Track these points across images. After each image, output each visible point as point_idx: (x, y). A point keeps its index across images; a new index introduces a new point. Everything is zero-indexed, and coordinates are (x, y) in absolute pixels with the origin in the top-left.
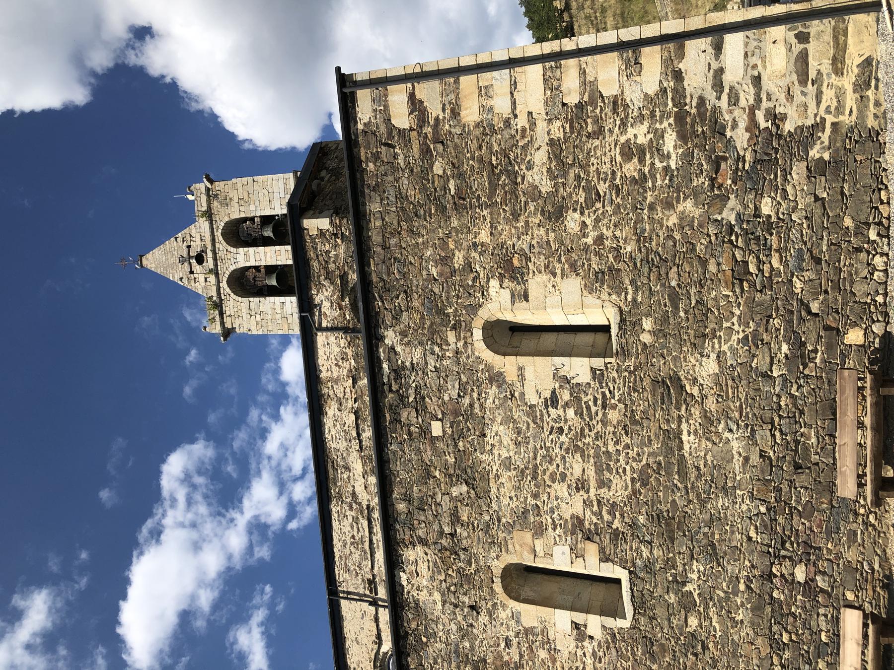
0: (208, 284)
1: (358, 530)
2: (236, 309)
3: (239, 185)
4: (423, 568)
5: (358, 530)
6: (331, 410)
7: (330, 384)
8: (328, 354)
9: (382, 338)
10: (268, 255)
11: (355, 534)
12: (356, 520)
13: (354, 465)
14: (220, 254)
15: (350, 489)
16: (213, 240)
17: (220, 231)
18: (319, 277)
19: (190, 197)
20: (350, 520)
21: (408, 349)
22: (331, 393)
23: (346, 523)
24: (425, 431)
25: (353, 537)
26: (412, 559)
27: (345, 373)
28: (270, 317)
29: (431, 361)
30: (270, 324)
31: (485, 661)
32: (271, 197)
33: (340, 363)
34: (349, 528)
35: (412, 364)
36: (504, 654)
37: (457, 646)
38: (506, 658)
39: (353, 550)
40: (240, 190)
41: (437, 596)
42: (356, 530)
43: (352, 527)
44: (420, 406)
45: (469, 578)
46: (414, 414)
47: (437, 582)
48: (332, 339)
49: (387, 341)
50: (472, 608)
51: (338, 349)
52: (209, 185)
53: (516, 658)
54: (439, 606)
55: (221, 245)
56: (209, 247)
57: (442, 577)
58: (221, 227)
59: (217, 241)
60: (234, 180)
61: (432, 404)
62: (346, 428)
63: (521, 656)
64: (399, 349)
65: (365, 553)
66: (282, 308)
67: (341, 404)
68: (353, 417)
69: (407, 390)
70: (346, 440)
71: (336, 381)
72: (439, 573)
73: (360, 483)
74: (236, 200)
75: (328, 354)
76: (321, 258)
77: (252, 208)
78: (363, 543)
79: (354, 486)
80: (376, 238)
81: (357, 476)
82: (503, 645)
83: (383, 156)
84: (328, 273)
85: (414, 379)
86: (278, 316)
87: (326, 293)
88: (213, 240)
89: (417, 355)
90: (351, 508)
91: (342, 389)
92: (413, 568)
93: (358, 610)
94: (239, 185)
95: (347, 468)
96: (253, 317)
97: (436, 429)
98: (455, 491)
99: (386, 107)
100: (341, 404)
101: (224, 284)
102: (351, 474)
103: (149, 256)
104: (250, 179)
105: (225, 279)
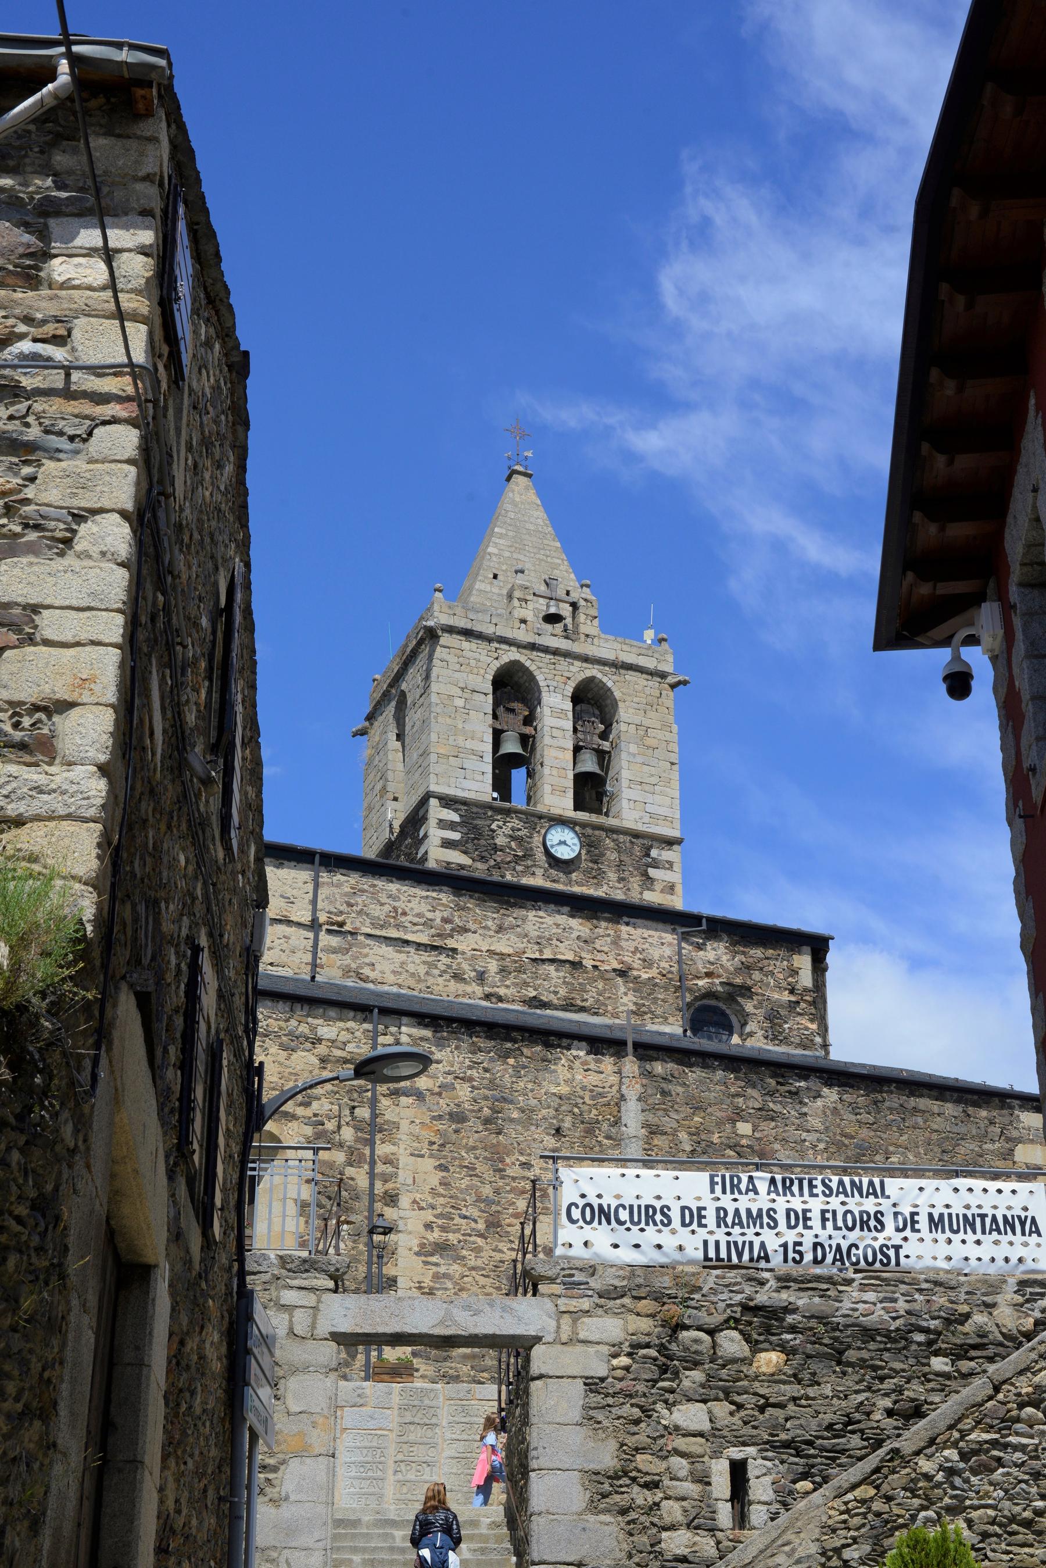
0: (517, 624)
1: (415, 924)
2: (473, 663)
3: (668, 736)
4: (593, 1079)
5: (415, 924)
6: (578, 926)
7: (612, 932)
8: (650, 940)
9: (829, 1084)
10: (560, 754)
11: (409, 918)
12: (428, 924)
13: (504, 942)
14: (563, 663)
15: (471, 926)
16: (586, 659)
17: (599, 676)
18: (744, 953)
19: (649, 635)
20: (430, 915)
21: (819, 1112)
22: (600, 931)
23: (424, 908)
24: (739, 1115)
25: (404, 914)
26: (602, 1067)
27: (626, 959)
28: (460, 726)
29: (811, 1137)
30: (449, 721)
31: (499, 1133)
32: (647, 788)
33: (638, 955)
34: (416, 911)
35: (805, 1114)
36: (513, 1159)
37: (511, 1102)
38: (508, 1160)
39: (387, 908)
40: (660, 734)
41: (564, 1090)
42: (416, 920)
43: (418, 915)
44: (766, 1114)
45: (590, 1132)
46: (757, 1105)
47: (582, 1093)
48: (668, 951)
49: (826, 1091)
50: (558, 1130)
51: (656, 958)
52: (671, 680)
53: (509, 1172)
54: (554, 1090)
55: (580, 672)
56: (577, 648)
57: (587, 1100)
58: (605, 679)
59: (585, 665)
60: (675, 728)
61: (768, 1128)
62: (554, 942)
63: (514, 1179)
64: (819, 1102)
65: (382, 927)
66: (473, 752)
67: (586, 941)
68: (570, 956)
69: (781, 1102)
70: (539, 937)
71: (616, 942)
72: (593, 1098)
73: (480, 942)
74: (647, 722)
75: (650, 940)
76: (766, 962)
77: (633, 748)
78: (398, 926)
79: (475, 932)
80: (924, 1103)
81: (490, 940)
82: (523, 1159)
83: (991, 1129)
84: (748, 968)
85: (791, 1111)
86: (460, 741)
87: (725, 958)
88: (586, 659)
89: (815, 1122)
90: (445, 921)
91: (606, 949)
92: (592, 1066)
93: (295, 892)
94: (668, 736)
95: (500, 929)
96: (459, 692)
97: (744, 1128)
98: (683, 1136)
99: (1032, 1141)
100: (586, 941)
101: (512, 655)
102: (492, 933)
103: (532, 496)
104: (674, 757)
105: (522, 659)
